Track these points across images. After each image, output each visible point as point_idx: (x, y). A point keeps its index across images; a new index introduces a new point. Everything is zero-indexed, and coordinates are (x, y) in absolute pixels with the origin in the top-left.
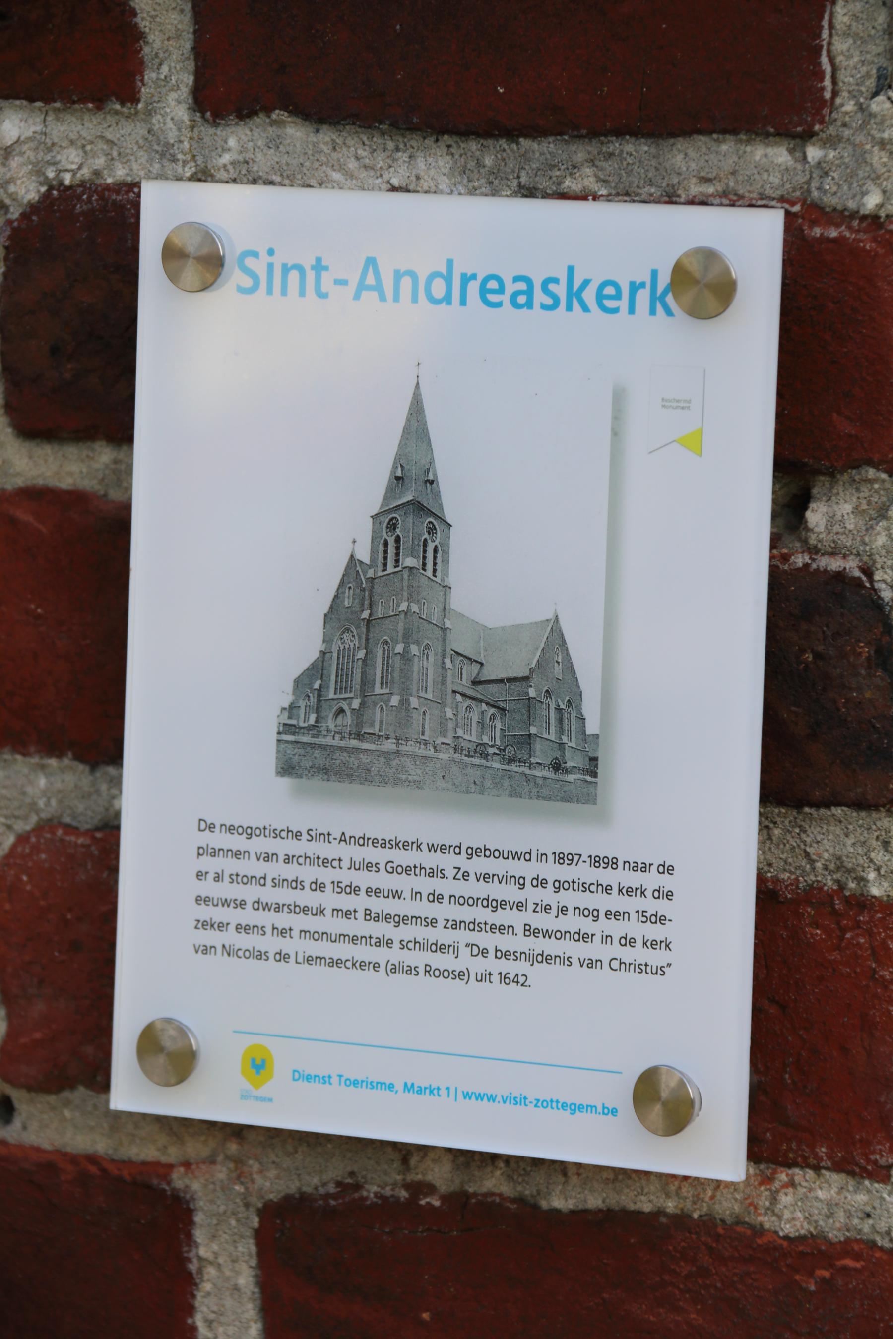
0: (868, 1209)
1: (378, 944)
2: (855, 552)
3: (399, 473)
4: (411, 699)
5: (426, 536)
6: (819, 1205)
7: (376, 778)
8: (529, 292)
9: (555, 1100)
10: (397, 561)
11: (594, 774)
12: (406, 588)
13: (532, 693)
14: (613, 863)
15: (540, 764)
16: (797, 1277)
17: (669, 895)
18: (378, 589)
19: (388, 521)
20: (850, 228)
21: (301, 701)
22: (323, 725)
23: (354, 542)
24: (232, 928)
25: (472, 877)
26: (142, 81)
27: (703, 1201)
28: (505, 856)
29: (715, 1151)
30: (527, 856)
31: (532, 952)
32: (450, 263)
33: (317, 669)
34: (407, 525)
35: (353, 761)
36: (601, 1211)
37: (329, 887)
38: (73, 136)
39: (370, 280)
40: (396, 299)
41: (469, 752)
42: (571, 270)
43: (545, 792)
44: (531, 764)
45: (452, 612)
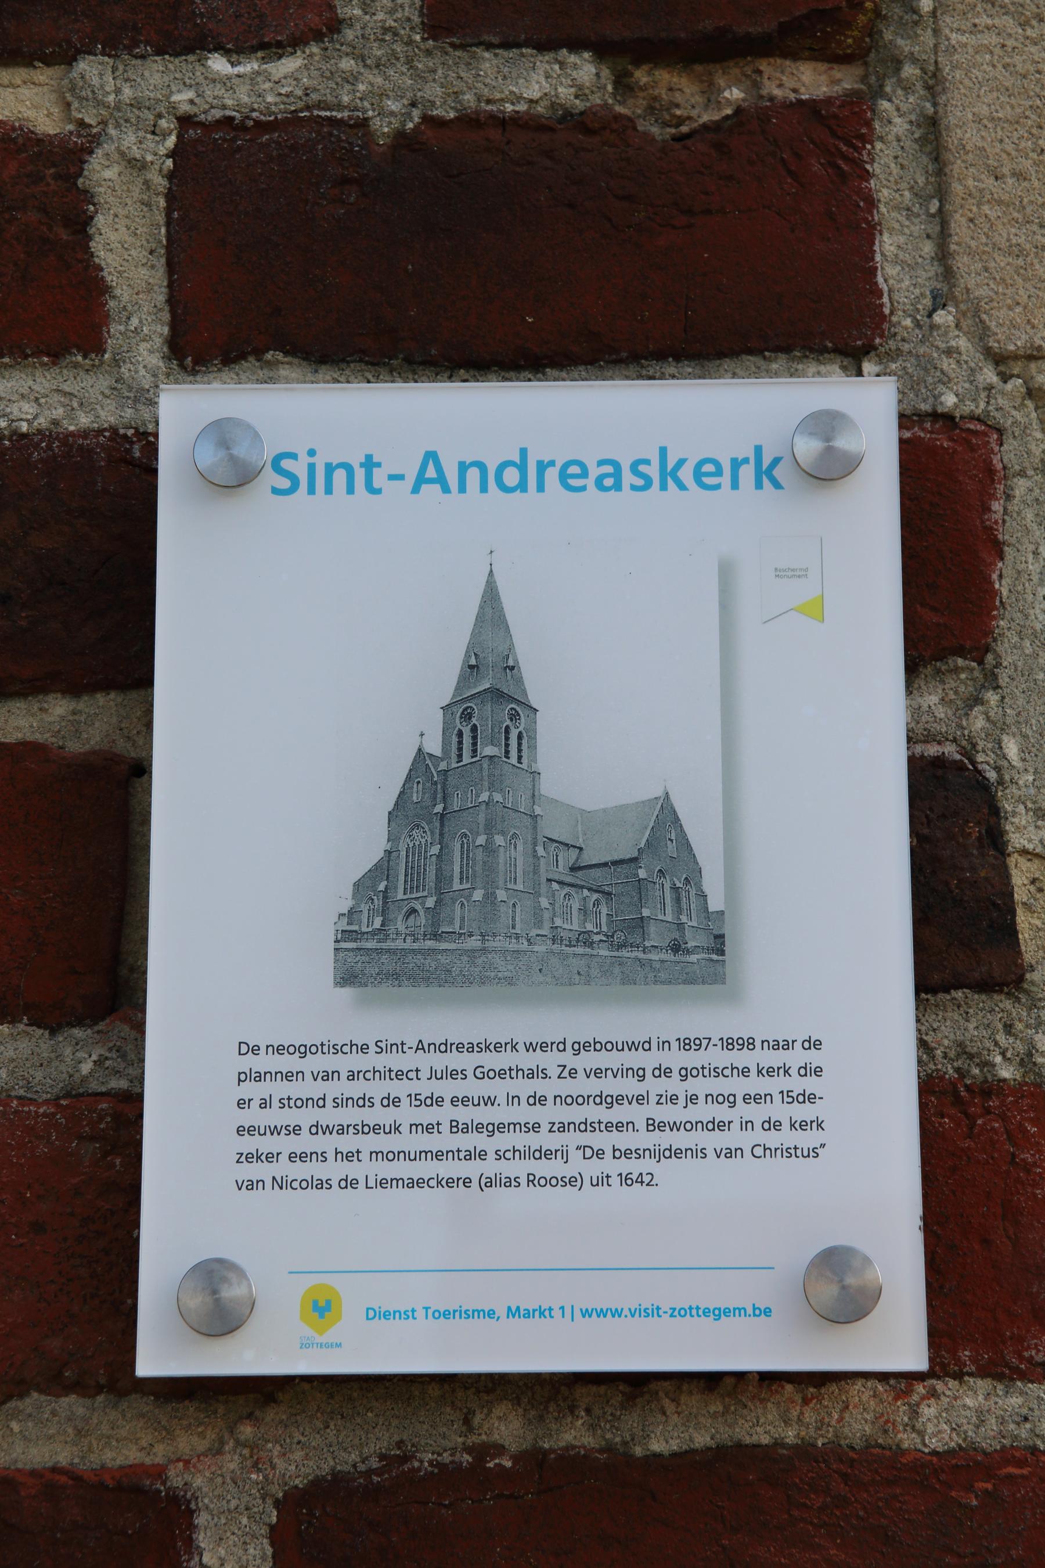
0: (1024, 1411)
1: (469, 1156)
2: (951, 737)
3: (473, 662)
4: (497, 891)
5: (508, 722)
6: (968, 1413)
7: (459, 979)
8: (617, 474)
9: (694, 1306)
10: (475, 751)
11: (722, 953)
12: (486, 778)
13: (642, 874)
14: (749, 1044)
15: (656, 947)
16: (953, 1494)
17: (818, 1071)
18: (452, 780)
19: (461, 712)
20: (923, 429)
21: (363, 905)
22: (391, 929)
23: (422, 735)
24: (284, 1158)
25: (581, 1074)
26: (108, 332)
27: (829, 1425)
28: (620, 1048)
29: (897, 1337)
30: (646, 1045)
31: (657, 1148)
32: (523, 452)
33: (383, 869)
34: (485, 715)
35: (430, 963)
36: (709, 1449)
37: (405, 1101)
38: (25, 390)
39: (431, 472)
40: (462, 489)
41: (570, 941)
42: (663, 452)
43: (662, 975)
44: (645, 948)
45: (543, 799)
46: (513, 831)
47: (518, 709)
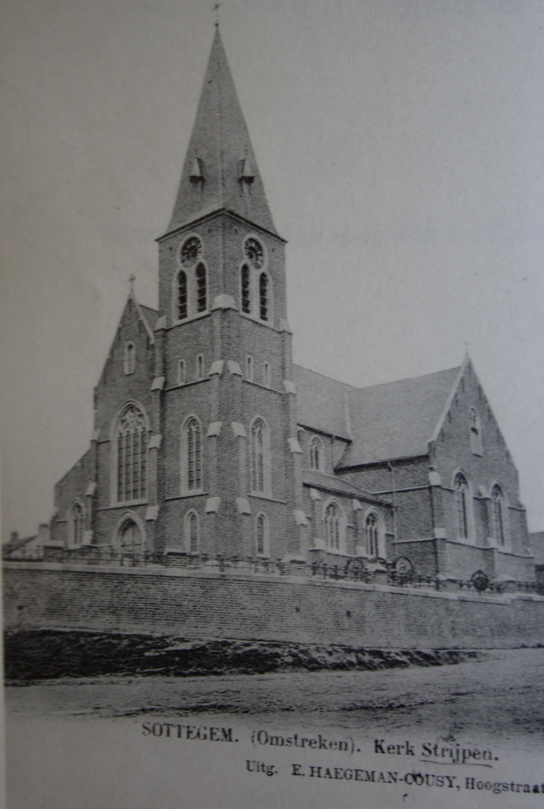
3: (196, 171)
5: (246, 260)
10: (202, 302)
13: (435, 479)
18: (175, 344)
23: (132, 279)
33: (90, 465)
44: (438, 582)
46: (258, 416)
47: (262, 243)
